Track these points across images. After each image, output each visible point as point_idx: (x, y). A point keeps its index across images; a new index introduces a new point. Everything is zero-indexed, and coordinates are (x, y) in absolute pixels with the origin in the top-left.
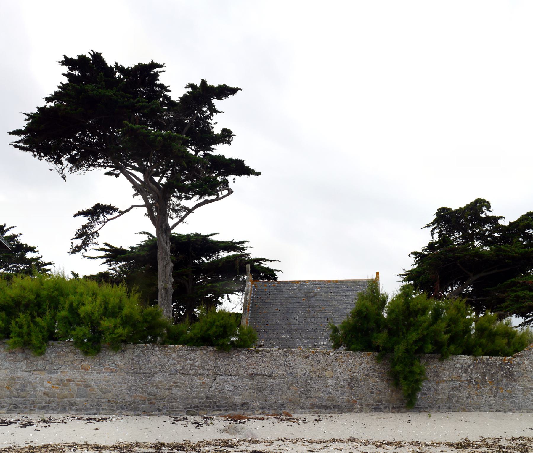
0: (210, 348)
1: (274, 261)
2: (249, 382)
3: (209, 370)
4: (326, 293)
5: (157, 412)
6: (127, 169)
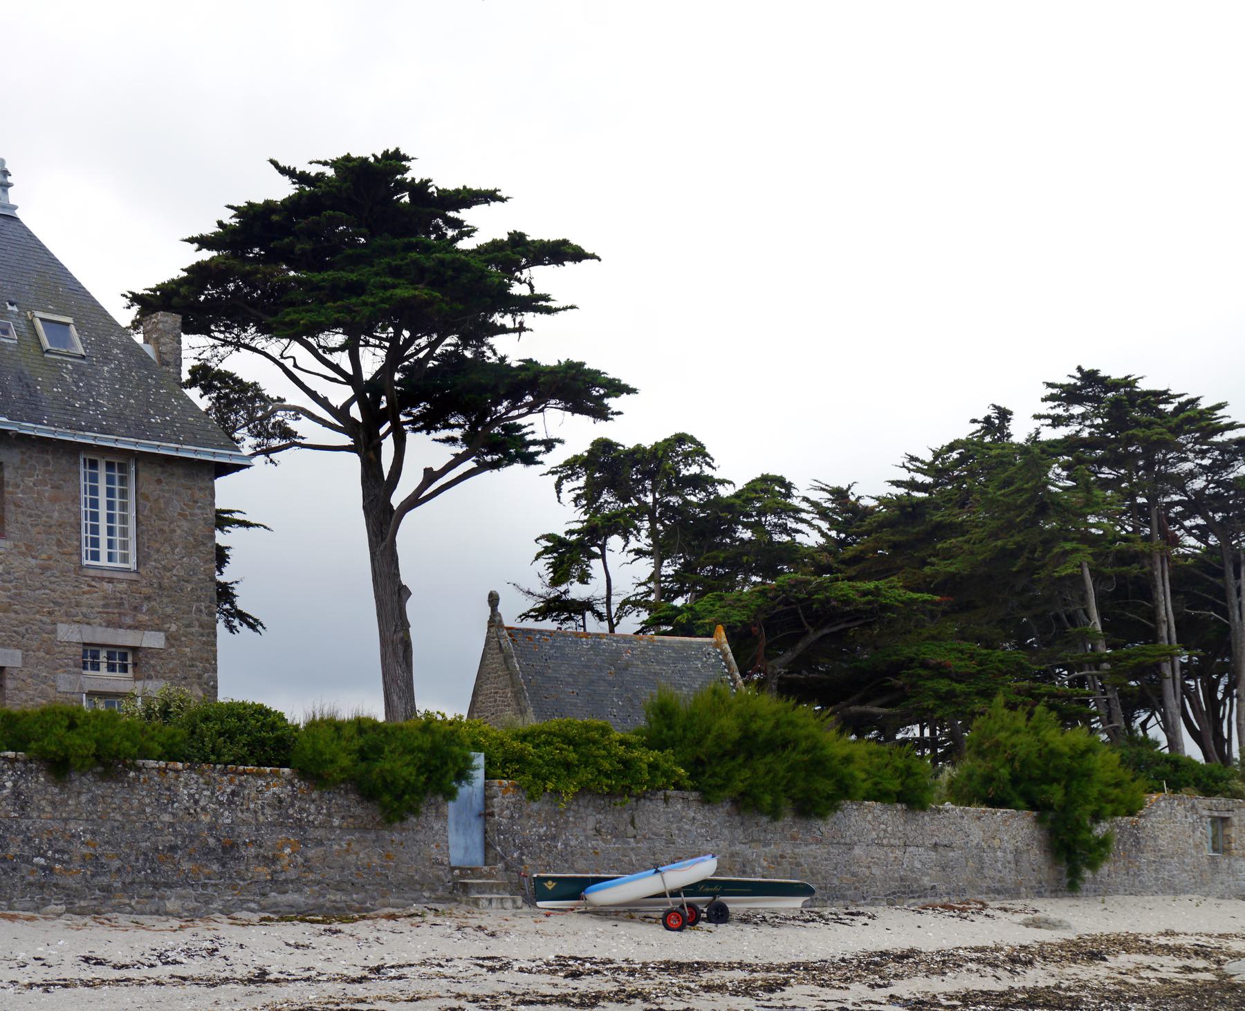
0: (899, 806)
1: (257, 525)
2: (933, 854)
3: (900, 838)
4: (644, 662)
5: (863, 902)
6: (412, 355)
